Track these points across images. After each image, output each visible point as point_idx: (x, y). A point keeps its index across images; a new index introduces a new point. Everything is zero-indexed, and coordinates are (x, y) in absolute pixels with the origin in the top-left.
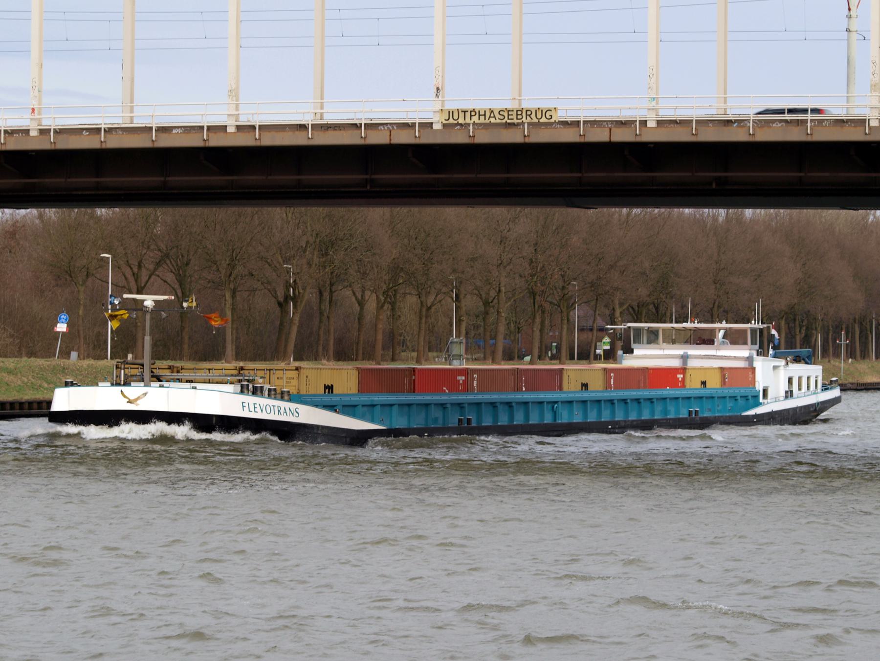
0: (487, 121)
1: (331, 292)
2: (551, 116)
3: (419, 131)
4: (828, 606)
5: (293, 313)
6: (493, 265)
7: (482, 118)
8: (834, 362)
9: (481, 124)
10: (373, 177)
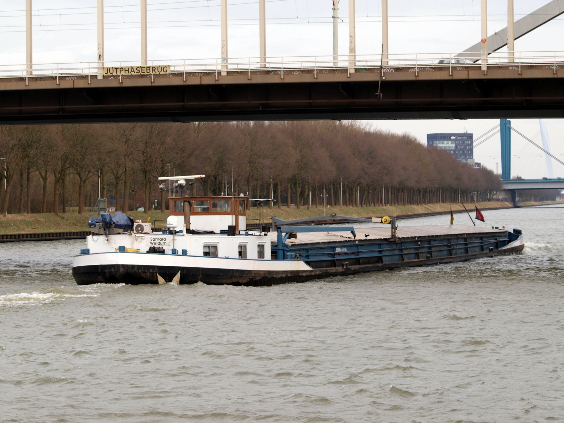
0: (130, 74)
1: (29, 173)
2: (167, 70)
3: (90, 80)
4: (229, 335)
5: (7, 186)
6: (121, 155)
7: (127, 72)
8: (319, 207)
9: (125, 76)
10: (64, 107)
